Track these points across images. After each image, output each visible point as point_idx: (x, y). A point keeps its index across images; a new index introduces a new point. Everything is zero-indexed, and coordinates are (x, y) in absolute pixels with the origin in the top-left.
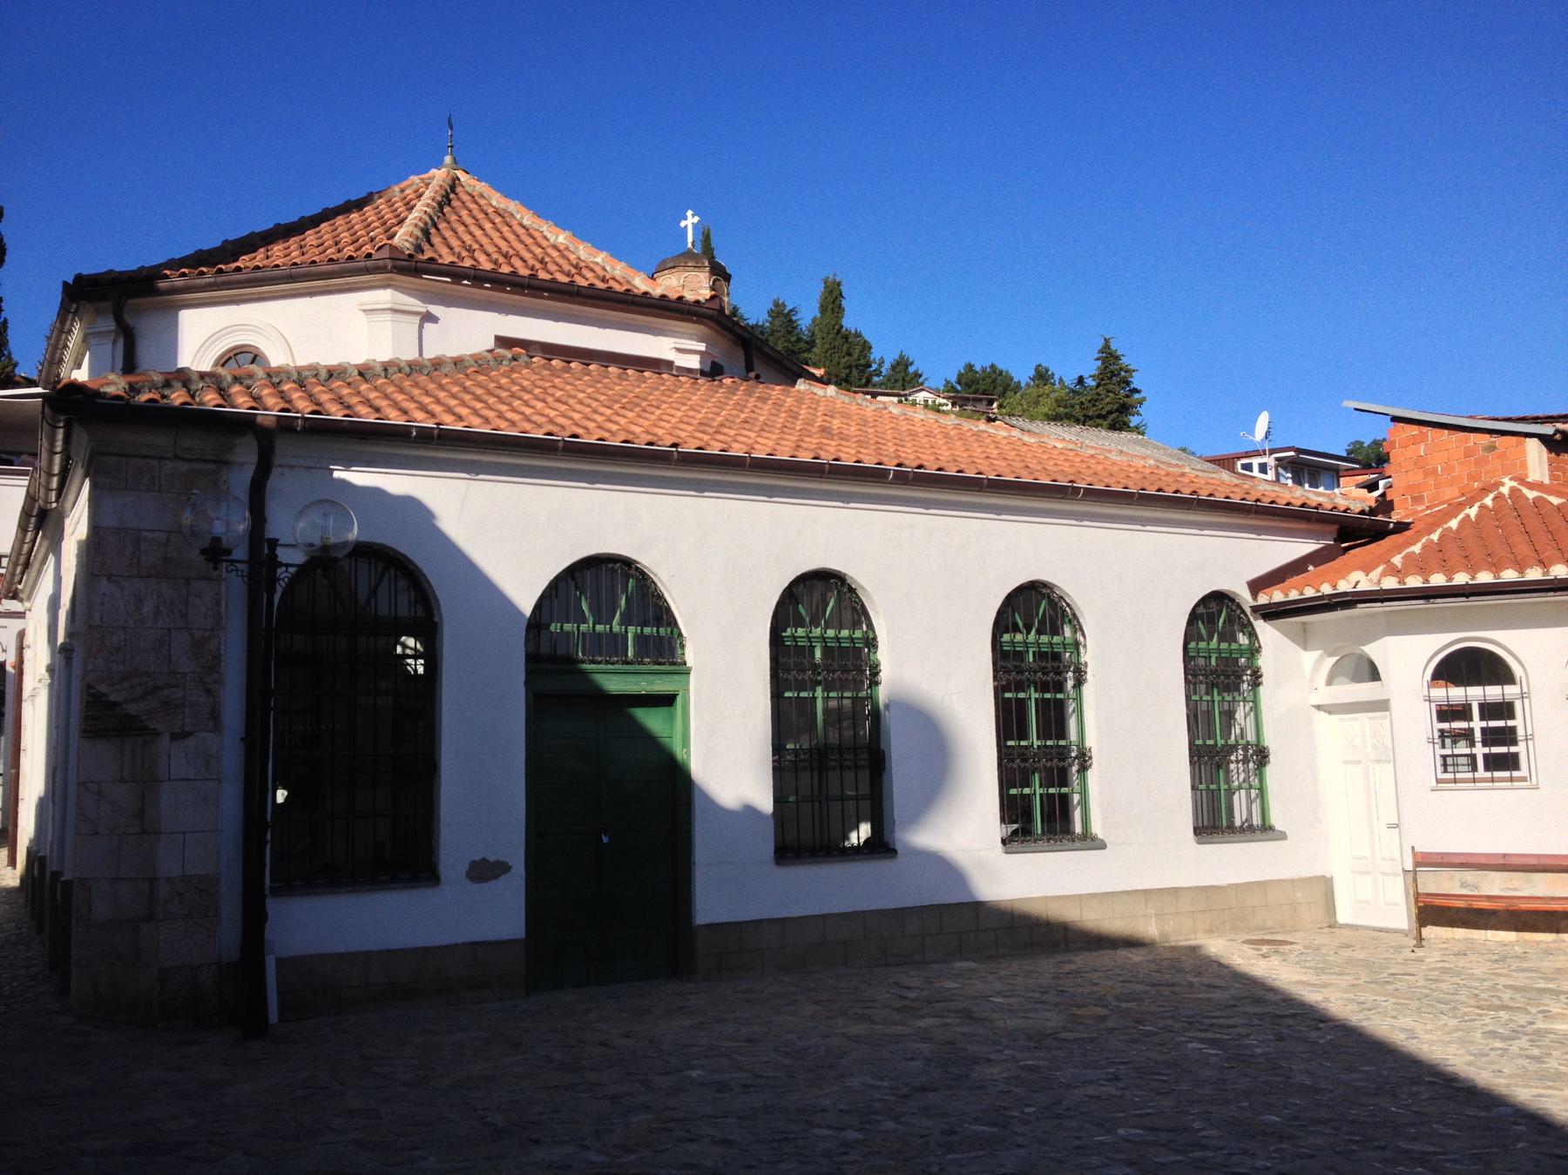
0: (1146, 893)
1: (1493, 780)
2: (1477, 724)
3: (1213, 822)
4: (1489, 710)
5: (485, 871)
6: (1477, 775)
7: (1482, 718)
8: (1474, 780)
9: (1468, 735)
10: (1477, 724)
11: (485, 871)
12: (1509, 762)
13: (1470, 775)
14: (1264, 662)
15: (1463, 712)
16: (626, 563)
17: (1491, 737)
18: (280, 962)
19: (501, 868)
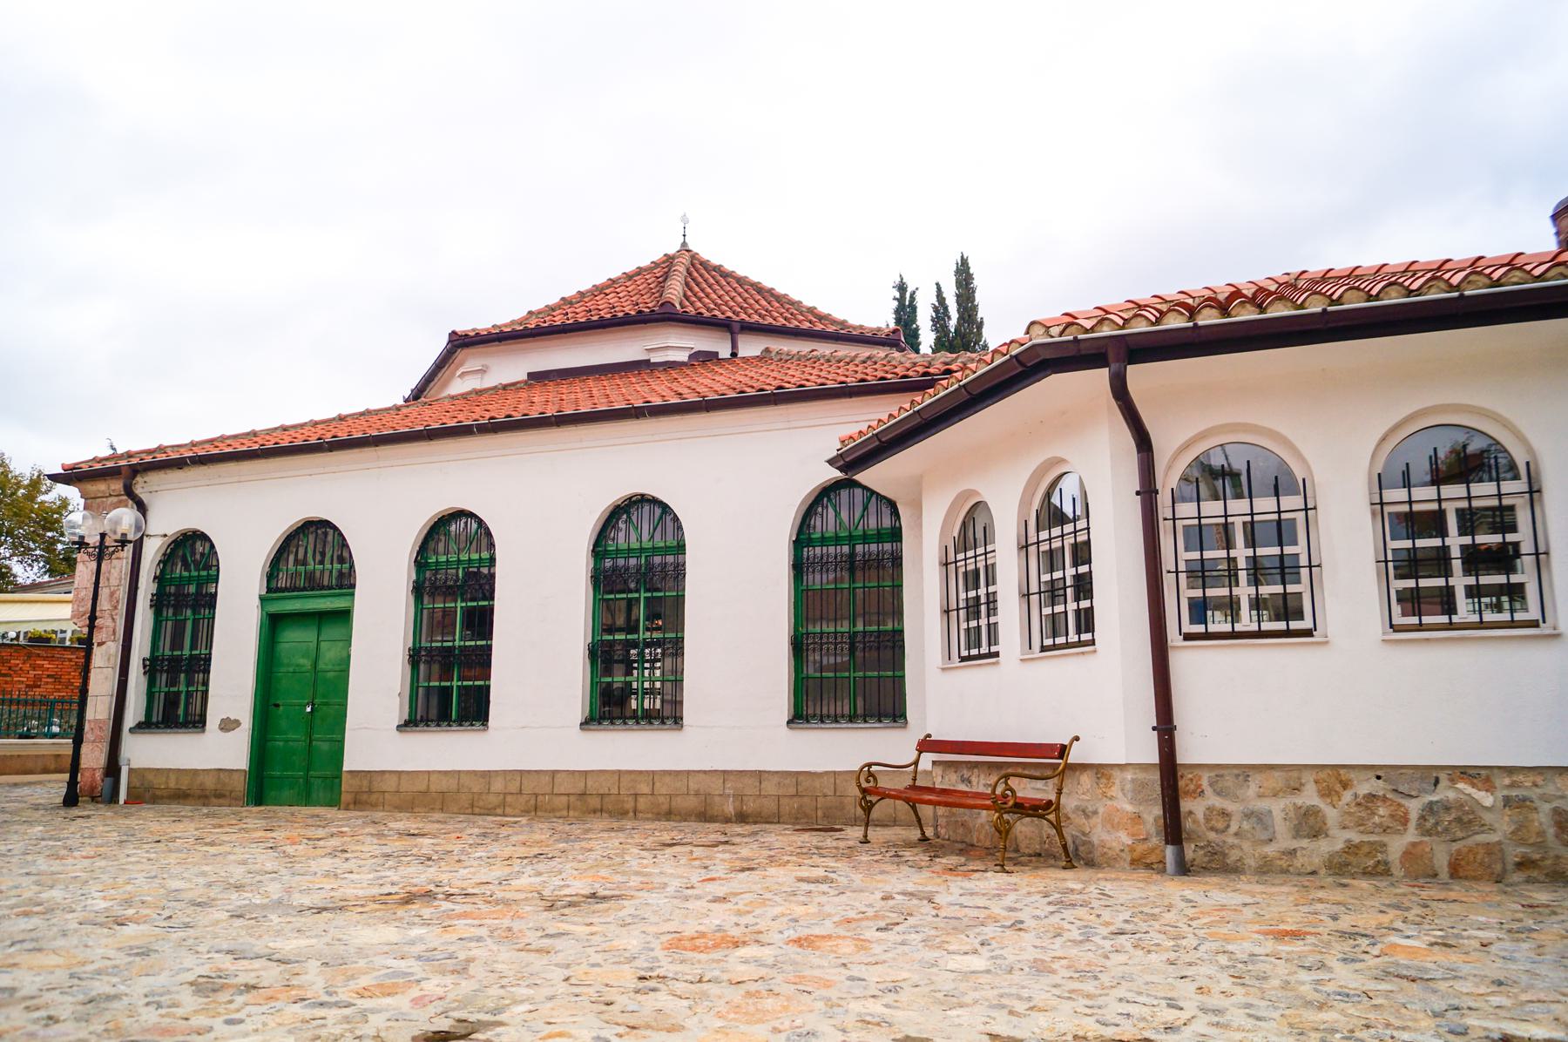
0: (446, 773)
1: (1420, 627)
2: (1455, 541)
3: (609, 707)
4: (1469, 520)
5: (228, 725)
6: (1455, 619)
7: (1463, 532)
8: (1451, 626)
9: (1257, 571)
10: (1455, 541)
11: (228, 725)
12: (1288, 609)
13: (1444, 619)
14: (1448, 449)
15: (1433, 523)
16: (326, 524)
17: (1475, 559)
18: (131, 771)
19: (237, 723)
